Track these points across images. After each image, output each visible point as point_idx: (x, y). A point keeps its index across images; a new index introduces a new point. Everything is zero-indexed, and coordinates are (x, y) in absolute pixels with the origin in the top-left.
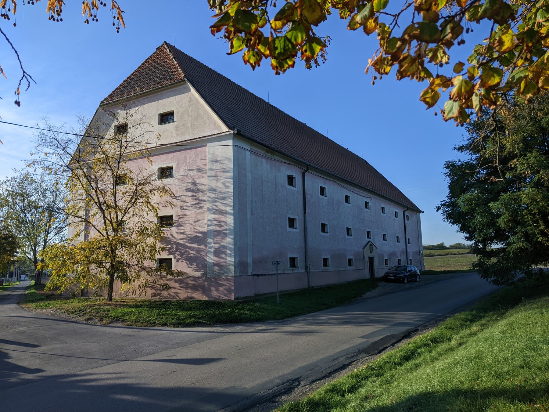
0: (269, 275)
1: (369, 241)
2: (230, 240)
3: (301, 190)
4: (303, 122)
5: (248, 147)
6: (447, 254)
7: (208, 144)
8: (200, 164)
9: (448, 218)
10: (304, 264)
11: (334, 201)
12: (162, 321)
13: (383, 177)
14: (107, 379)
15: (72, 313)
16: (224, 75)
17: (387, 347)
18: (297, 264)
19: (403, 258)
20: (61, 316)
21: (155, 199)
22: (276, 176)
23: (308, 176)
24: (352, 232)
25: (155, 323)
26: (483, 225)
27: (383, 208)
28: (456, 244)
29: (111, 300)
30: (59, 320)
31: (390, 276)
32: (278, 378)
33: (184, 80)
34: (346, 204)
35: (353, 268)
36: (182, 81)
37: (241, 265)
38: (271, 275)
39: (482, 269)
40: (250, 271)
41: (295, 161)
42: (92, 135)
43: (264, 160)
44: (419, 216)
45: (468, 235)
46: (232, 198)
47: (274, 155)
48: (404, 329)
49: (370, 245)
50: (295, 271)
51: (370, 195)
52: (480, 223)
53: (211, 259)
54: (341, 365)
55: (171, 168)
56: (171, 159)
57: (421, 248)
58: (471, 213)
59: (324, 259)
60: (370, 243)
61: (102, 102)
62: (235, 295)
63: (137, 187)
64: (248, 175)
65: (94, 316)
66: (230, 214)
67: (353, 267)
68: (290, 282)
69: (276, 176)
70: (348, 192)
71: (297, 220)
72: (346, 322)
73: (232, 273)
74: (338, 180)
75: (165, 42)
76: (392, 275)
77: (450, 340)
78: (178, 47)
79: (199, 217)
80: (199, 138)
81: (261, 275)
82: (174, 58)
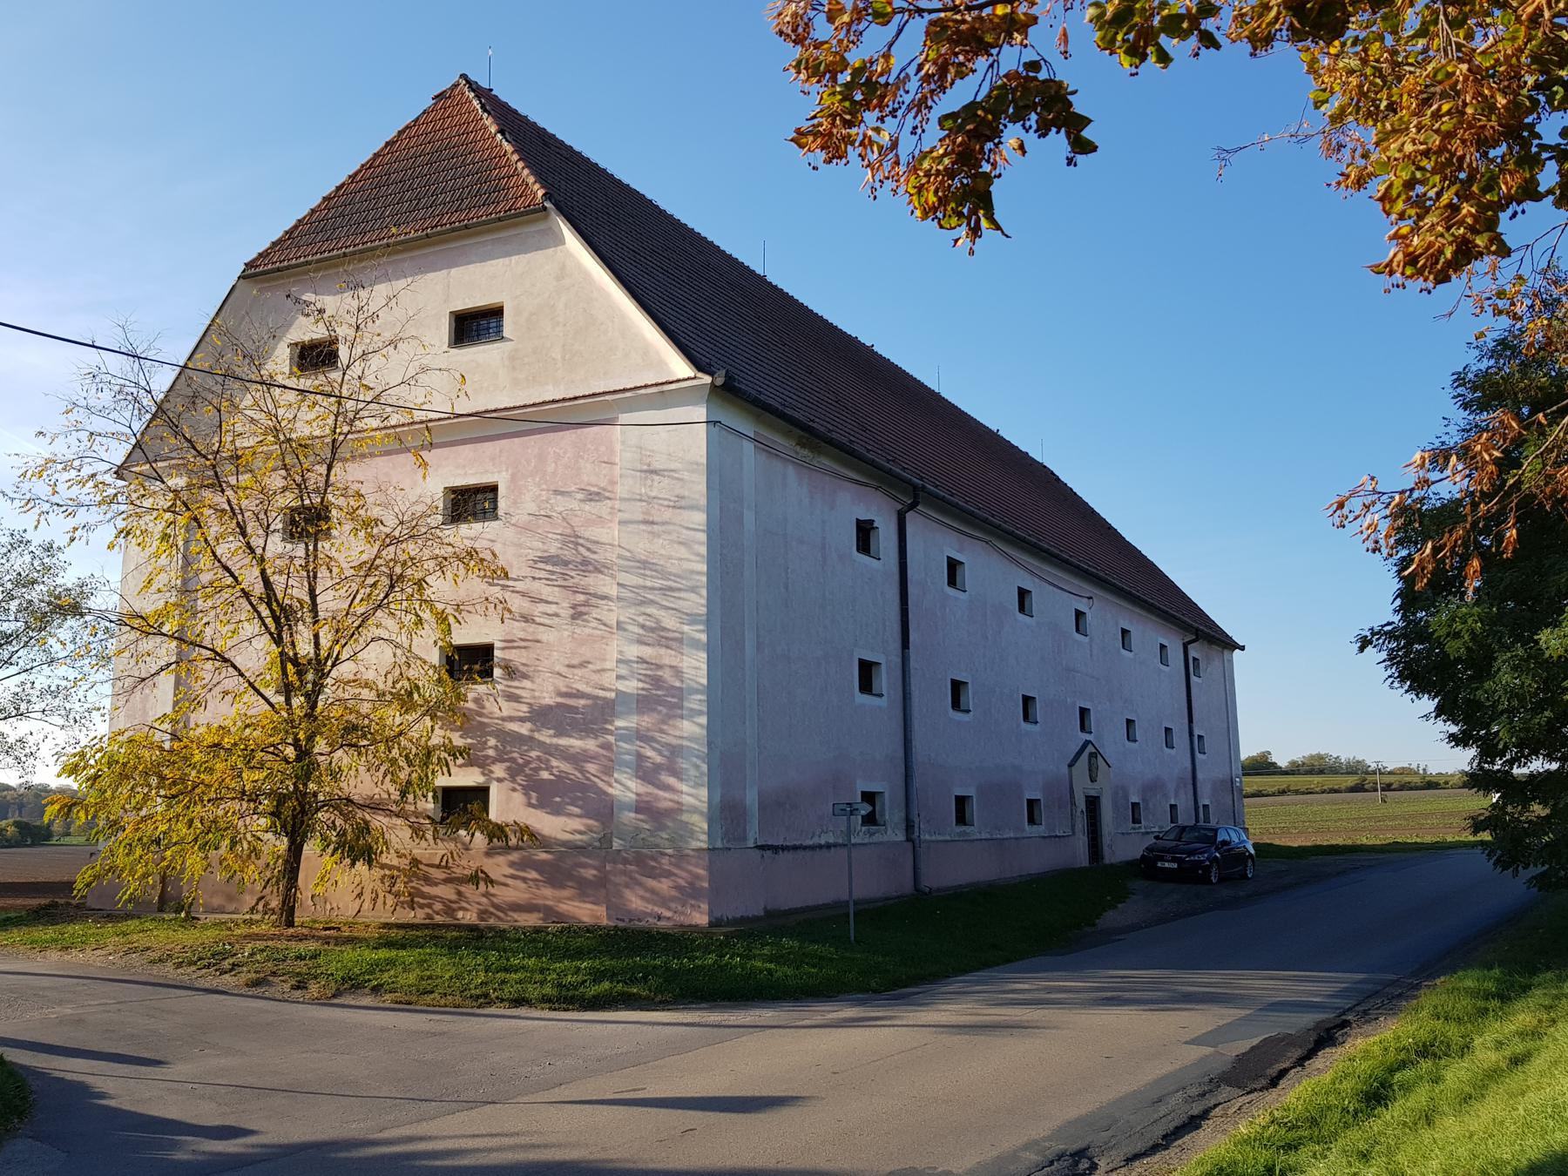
0: (805, 848)
1: (1087, 743)
2: (697, 730)
3: (895, 569)
4: (866, 340)
5: (746, 426)
6: (1283, 792)
7: (624, 418)
8: (591, 475)
9: (1402, 678)
10: (903, 815)
11: (985, 600)
12: (508, 991)
13: (1110, 527)
14: (490, 1150)
15: (191, 963)
16: (633, 186)
17: (1283, 1073)
18: (883, 815)
19: (1184, 803)
20: (155, 969)
21: (440, 588)
22: (824, 522)
23: (914, 522)
24: (1039, 710)
25: (486, 996)
26: (1522, 699)
27: (1125, 632)
28: (1312, 757)
29: (290, 924)
30: (160, 985)
31: (1163, 859)
32: (1027, 1147)
33: (545, 209)
34: (1021, 617)
35: (1040, 830)
36: (535, 211)
37: (727, 813)
38: (812, 848)
39: (1507, 841)
40: (753, 835)
41: (881, 476)
42: (218, 366)
43: (791, 469)
44: (1231, 662)
45: (1454, 729)
46: (704, 592)
47: (820, 453)
48: (1308, 1019)
49: (1091, 755)
50: (876, 838)
51: (1088, 589)
52: (1513, 694)
53: (625, 788)
54: (1184, 1118)
55: (493, 489)
56: (493, 459)
57: (1237, 770)
58: (1481, 663)
59: (957, 798)
60: (1090, 749)
61: (249, 265)
62: (710, 913)
63: (385, 546)
64: (749, 517)
65: (274, 974)
66: (695, 644)
67: (1042, 828)
68: (864, 874)
69: (824, 522)
70: (1027, 576)
71: (883, 667)
72: (1108, 999)
73: (701, 842)
74: (999, 537)
75: (464, 76)
76: (1169, 856)
77: (1465, 1049)
78: (501, 93)
79: (586, 652)
80: (594, 395)
81: (784, 848)
82: (502, 132)
